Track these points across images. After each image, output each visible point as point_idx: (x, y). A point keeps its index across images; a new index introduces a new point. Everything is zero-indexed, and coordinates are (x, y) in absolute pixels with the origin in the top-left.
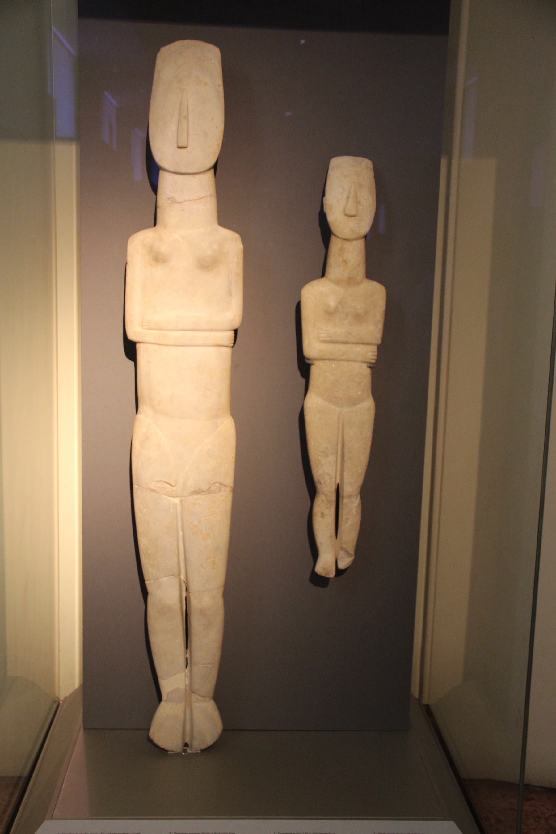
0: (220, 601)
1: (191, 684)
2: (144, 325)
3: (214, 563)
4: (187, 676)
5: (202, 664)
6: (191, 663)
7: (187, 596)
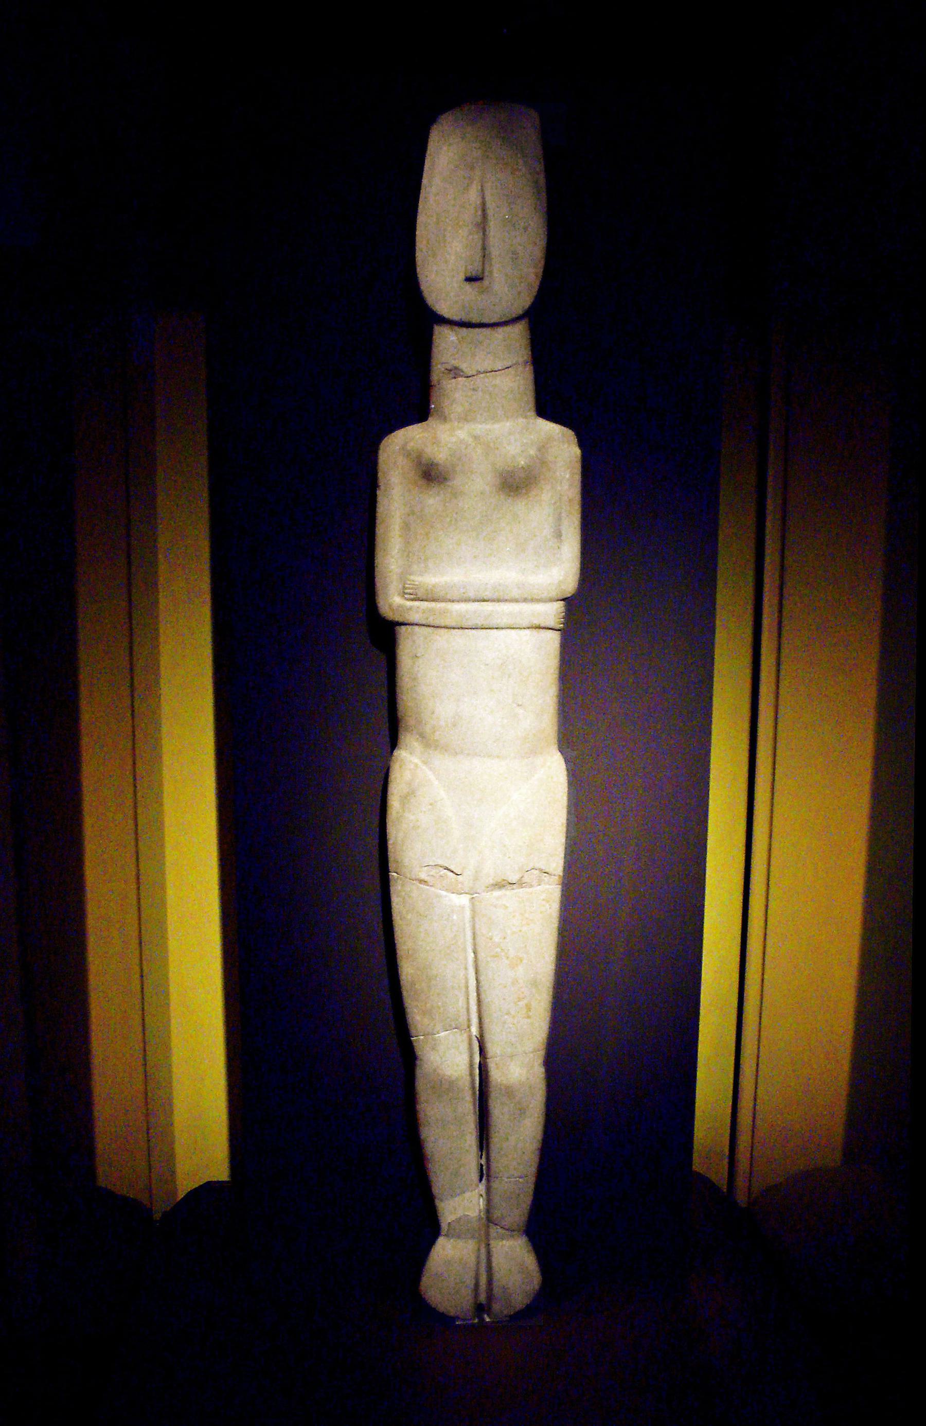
0: (539, 1071)
1: (488, 1211)
2: (406, 594)
3: (528, 1007)
4: (481, 1195)
5: (507, 1178)
6: (488, 1176)
7: (482, 1062)
